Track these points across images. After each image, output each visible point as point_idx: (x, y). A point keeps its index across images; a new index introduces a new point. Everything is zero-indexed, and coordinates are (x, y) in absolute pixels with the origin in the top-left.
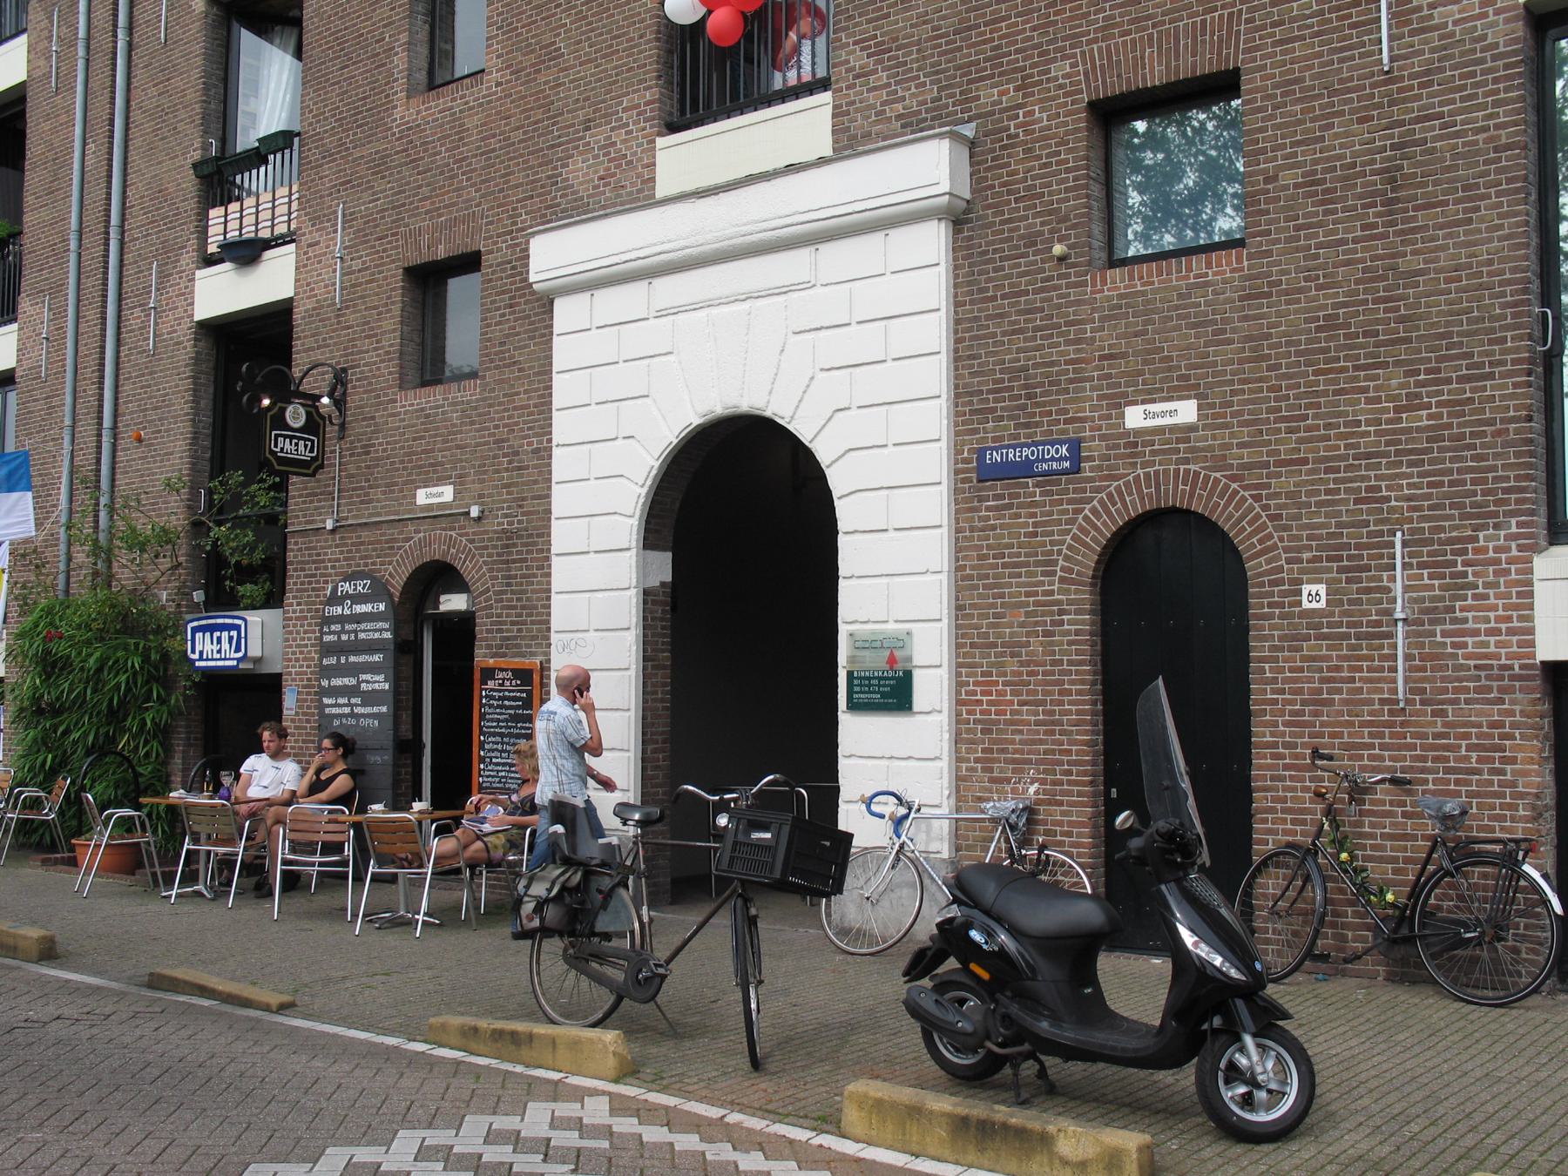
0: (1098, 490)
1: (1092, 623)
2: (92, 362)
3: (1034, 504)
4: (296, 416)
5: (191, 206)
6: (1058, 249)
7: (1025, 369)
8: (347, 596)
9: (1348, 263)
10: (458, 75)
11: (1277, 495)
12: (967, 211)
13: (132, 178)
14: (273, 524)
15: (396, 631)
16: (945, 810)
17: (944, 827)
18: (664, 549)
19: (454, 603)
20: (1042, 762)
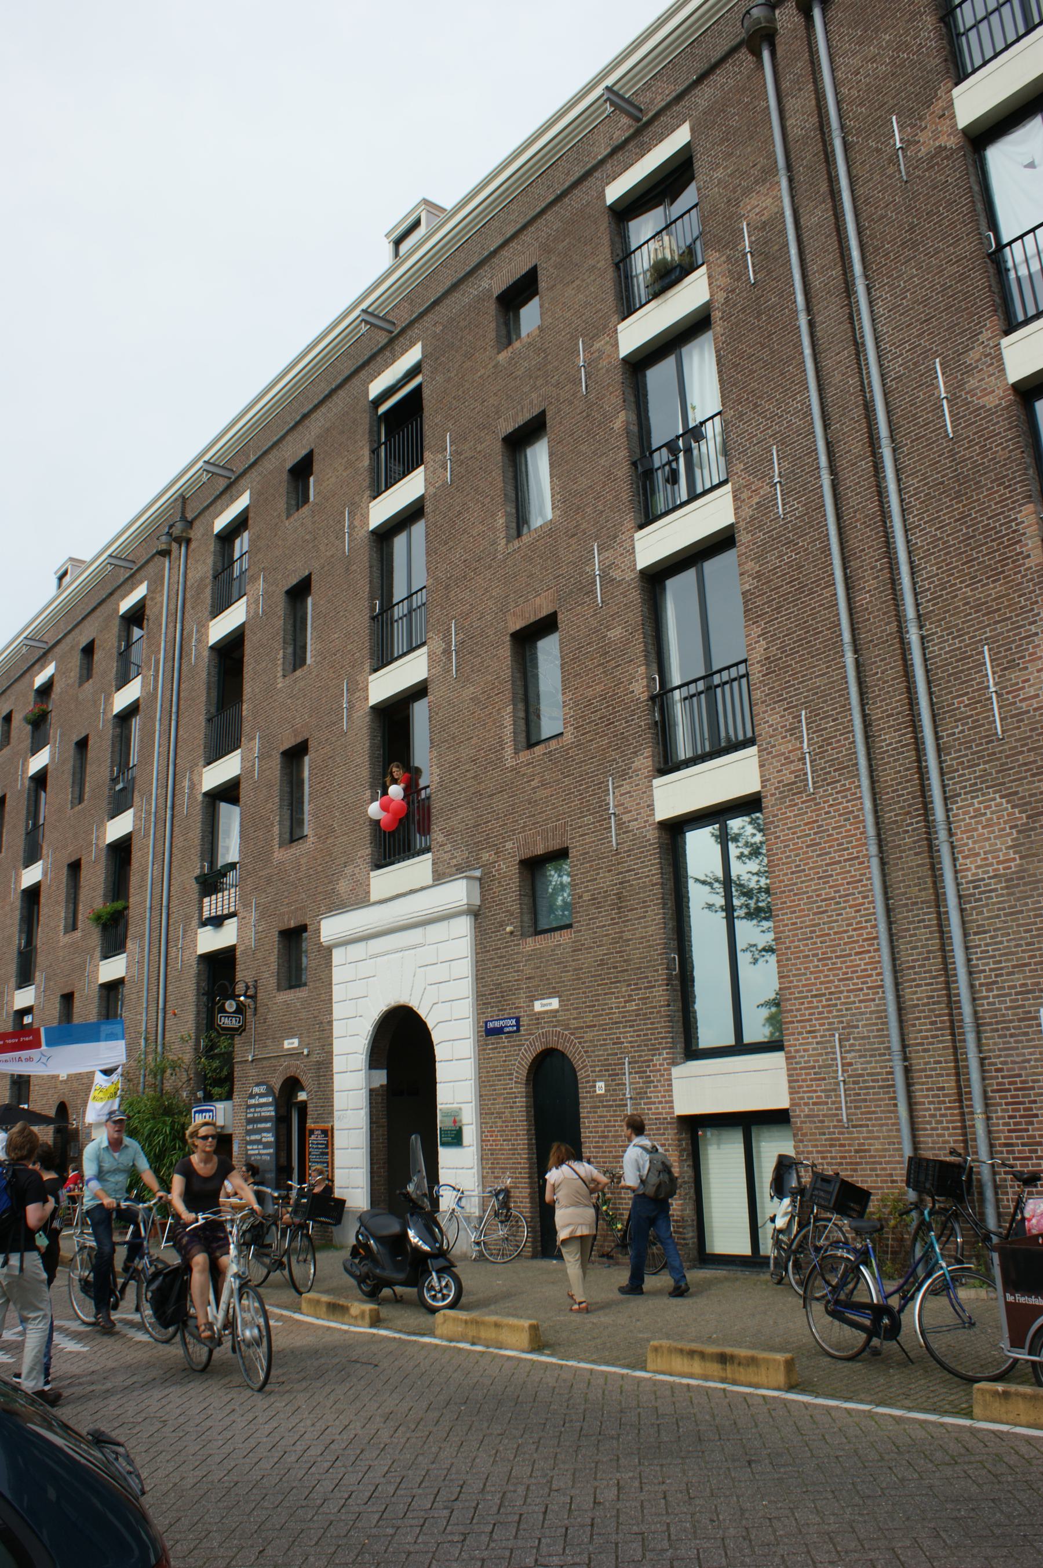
0: (526, 1040)
1: (527, 1102)
2: (154, 975)
3: (504, 1047)
4: (231, 1006)
5: (196, 896)
6: (509, 929)
7: (500, 984)
8: (257, 1094)
9: (606, 935)
10: (544, 736)
11: (586, 1042)
12: (479, 910)
13: (173, 882)
14: (228, 1059)
15: (277, 1111)
16: (476, 1193)
17: (476, 1200)
18: (382, 1068)
19: (302, 1096)
20: (511, 1168)
